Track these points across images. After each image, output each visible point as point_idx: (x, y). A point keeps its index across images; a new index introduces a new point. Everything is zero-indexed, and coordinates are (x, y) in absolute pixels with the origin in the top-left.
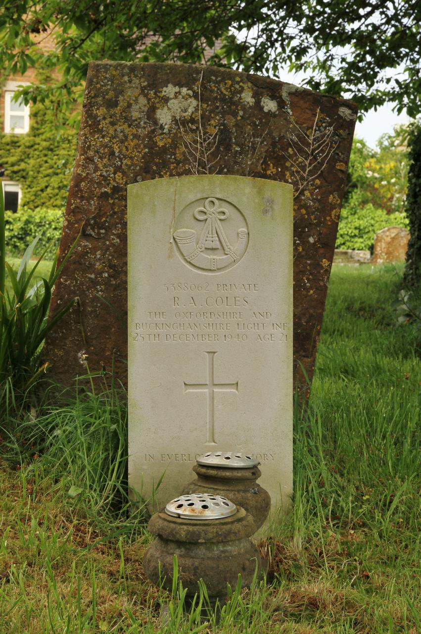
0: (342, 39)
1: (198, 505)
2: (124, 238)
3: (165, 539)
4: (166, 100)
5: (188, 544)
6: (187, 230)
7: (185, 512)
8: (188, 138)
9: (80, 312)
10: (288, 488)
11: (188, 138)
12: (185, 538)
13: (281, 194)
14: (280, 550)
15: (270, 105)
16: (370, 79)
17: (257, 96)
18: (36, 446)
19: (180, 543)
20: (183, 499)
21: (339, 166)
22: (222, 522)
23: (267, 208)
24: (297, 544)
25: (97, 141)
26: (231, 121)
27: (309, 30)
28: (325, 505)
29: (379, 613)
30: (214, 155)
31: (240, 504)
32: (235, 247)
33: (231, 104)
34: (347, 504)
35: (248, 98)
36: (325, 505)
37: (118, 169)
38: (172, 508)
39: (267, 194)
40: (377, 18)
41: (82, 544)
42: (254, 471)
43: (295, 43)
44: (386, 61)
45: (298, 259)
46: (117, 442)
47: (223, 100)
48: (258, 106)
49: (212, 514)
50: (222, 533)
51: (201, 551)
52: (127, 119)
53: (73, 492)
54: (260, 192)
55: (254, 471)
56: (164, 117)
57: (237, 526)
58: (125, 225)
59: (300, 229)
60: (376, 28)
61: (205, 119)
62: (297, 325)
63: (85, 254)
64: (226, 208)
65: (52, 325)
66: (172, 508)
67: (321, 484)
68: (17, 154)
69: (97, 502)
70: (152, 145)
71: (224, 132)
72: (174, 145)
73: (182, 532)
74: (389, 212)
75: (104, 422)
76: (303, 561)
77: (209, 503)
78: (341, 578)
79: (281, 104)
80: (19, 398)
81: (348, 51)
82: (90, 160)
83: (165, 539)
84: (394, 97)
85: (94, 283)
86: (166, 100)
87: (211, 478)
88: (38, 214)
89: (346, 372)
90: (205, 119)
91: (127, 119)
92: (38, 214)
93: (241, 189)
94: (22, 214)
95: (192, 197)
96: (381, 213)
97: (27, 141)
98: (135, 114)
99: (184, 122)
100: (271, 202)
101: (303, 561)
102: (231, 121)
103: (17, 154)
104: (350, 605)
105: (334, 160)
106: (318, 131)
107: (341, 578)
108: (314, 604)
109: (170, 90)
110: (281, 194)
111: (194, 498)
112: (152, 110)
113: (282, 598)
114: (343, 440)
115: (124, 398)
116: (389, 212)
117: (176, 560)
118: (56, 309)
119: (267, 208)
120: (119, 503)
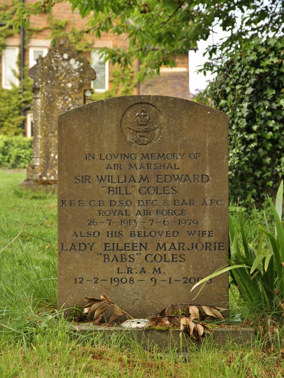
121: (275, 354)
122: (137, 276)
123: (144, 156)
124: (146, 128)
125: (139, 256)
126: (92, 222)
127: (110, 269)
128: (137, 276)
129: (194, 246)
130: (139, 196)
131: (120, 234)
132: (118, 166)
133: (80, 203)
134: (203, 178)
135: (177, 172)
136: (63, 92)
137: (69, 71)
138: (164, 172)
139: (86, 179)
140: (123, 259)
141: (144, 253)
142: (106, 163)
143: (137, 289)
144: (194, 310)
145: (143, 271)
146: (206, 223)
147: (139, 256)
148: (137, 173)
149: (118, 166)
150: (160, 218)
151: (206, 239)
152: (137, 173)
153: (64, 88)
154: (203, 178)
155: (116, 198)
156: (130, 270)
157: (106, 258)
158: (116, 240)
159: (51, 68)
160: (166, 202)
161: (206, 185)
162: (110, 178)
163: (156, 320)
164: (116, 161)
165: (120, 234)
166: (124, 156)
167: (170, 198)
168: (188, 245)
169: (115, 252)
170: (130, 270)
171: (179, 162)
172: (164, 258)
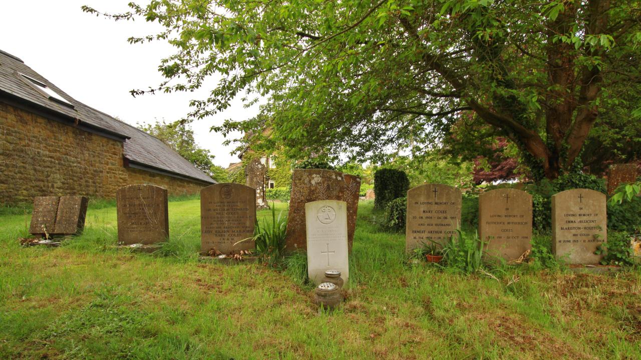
0: (356, 145)
1: (326, 286)
2: (304, 213)
3: (319, 295)
4: (313, 178)
5: (325, 296)
6: (321, 214)
7: (323, 288)
8: (319, 187)
9: (294, 231)
10: (348, 276)
11: (319, 187)
12: (324, 295)
13: (343, 204)
14: (346, 292)
15: (339, 178)
16: (363, 155)
17: (336, 176)
18: (285, 267)
19: (322, 296)
20: (322, 284)
21: (357, 193)
22: (332, 290)
23: (340, 208)
24: (350, 291)
25: (296, 189)
26: (330, 183)
27: (347, 144)
28: (357, 279)
29: (371, 309)
30: (326, 191)
31: (335, 284)
32: (333, 218)
33: (330, 178)
34: (362, 279)
35: (334, 177)
36: (357, 279)
37: (302, 196)
38: (320, 287)
39: (340, 204)
40: (364, 141)
41: (298, 293)
42: (340, 275)
43: (344, 147)
44: (367, 151)
45: (348, 216)
46: (305, 267)
47: (328, 177)
48: (336, 179)
49: (330, 288)
50: (332, 293)
51: (327, 298)
52: (304, 183)
53: (295, 280)
54: (338, 204)
55: (340, 275)
56: (313, 182)
57: (336, 291)
58: (304, 209)
59: (348, 209)
60: (364, 143)
61: (323, 182)
62: (348, 233)
63: (294, 217)
64: (330, 208)
65: (287, 235)
66: (320, 287)
67: (356, 274)
68: (273, 173)
69: (301, 282)
70: (310, 189)
71: (328, 186)
72: (316, 189)
73: (323, 293)
74: (369, 184)
75: (301, 262)
76: (352, 295)
77: (329, 285)
78: (362, 300)
79: (342, 178)
80: (280, 254)
81: (357, 149)
82: (295, 193)
83: (319, 295)
84: (369, 159)
85: (297, 224)
86: (313, 178)
87: (329, 277)
88: (279, 189)
89: (361, 239)
90: (323, 182)
91: (304, 183)
92: (279, 189)
93: (334, 203)
94: (275, 189)
95: (321, 206)
96: (367, 185)
97: (275, 170)
98: (306, 182)
99: (318, 183)
100: (341, 206)
101: (352, 295)
102: (330, 183)
103: (273, 173)
104: (364, 308)
105: (356, 191)
106: (352, 184)
107: (362, 300)
108: (355, 307)
109: (314, 175)
110: (343, 204)
111: (325, 284)
112: (310, 180)
113: (347, 307)
114: (361, 262)
115: (306, 254)
116: (369, 184)
117: (321, 299)
118: (288, 231)
119: (340, 208)
120: (306, 282)
121: (520, 274)
122: (226, 241)
123: (228, 202)
124: (228, 193)
125: (226, 234)
126: (211, 224)
127: (217, 239)
128: (226, 241)
129: (244, 231)
130: (226, 215)
131: (220, 228)
132: (220, 206)
133: (208, 218)
134: (246, 209)
135: (238, 208)
136: (256, 176)
137: (258, 169)
138: (234, 207)
139: (209, 210)
140: (221, 235)
141: (228, 234)
142: (215, 205)
143: (226, 245)
144: (242, 252)
145: (228, 239)
146: (248, 224)
147: (226, 234)
148: (226, 208)
149: (220, 206)
150: (233, 222)
151: (248, 229)
152: (226, 208)
153: (257, 174)
154: (246, 209)
155: (219, 216)
156: (224, 239)
157: (216, 235)
158: (219, 230)
159: (252, 168)
160: (235, 217)
161: (248, 212)
162: (217, 210)
163: (228, 255)
164: (219, 204)
165: (220, 228)
166: (221, 202)
167: (236, 216)
168: (242, 230)
169: (220, 234)
170: (224, 239)
171: (239, 204)
172: (235, 235)
